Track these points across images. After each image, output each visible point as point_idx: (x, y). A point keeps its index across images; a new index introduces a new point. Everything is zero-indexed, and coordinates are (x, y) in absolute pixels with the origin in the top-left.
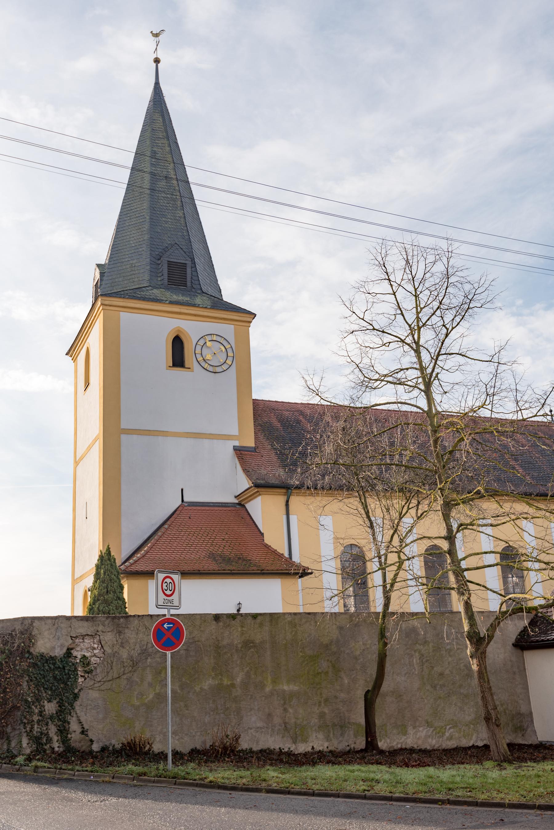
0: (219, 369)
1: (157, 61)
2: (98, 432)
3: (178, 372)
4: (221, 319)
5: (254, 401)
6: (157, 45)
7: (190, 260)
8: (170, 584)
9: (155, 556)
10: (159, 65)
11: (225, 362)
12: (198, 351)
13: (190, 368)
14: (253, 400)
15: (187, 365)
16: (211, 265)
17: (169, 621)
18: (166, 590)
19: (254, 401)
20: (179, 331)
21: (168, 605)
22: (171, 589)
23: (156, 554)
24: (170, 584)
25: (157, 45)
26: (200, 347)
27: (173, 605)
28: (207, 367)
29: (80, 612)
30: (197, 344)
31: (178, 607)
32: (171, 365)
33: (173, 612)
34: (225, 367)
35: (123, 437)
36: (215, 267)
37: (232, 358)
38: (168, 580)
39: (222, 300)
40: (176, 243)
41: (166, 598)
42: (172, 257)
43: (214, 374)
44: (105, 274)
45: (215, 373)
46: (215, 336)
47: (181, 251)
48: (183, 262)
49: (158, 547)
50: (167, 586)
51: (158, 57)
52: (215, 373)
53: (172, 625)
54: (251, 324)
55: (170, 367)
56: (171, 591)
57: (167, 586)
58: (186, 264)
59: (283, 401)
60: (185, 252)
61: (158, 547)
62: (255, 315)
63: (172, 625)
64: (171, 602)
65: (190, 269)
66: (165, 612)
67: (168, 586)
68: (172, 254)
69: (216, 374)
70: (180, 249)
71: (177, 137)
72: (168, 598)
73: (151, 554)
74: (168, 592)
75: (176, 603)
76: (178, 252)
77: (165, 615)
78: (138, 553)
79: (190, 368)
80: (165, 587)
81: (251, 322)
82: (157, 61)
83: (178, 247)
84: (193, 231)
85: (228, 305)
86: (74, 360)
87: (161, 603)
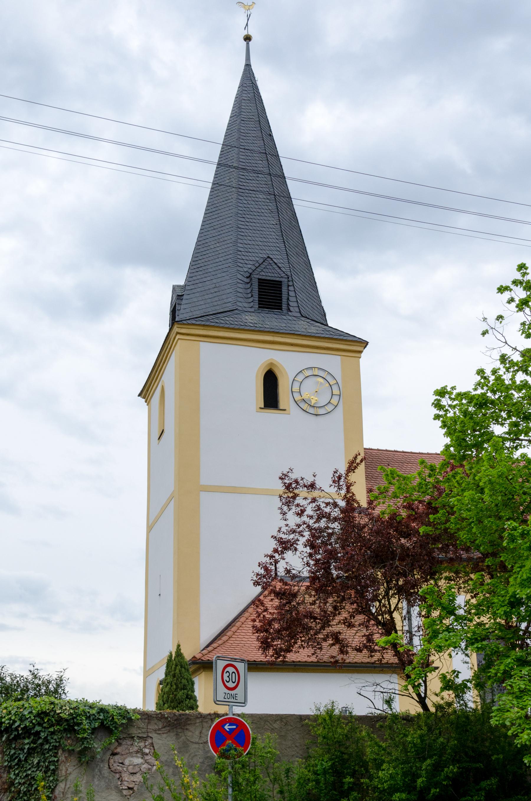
0: (321, 411)
1: (248, 38)
2: (172, 489)
3: (271, 414)
4: (292, 345)
5: (367, 451)
6: (248, 20)
7: (286, 277)
8: (234, 674)
9: (239, 642)
10: (250, 43)
11: (329, 402)
12: (296, 388)
13: (285, 410)
14: (365, 449)
15: (282, 405)
16: (313, 282)
17: (231, 721)
18: (228, 682)
19: (367, 451)
20: (272, 364)
21: (230, 700)
22: (234, 681)
23: (247, 640)
24: (234, 674)
25: (248, 20)
26: (298, 384)
27: (236, 701)
28: (307, 408)
29: (152, 707)
30: (294, 379)
31: (244, 703)
32: (263, 406)
33: (238, 710)
34: (329, 408)
35: (203, 495)
36: (318, 284)
37: (338, 397)
38: (231, 669)
39: (327, 325)
40: (268, 257)
41: (227, 691)
42: (263, 273)
43: (314, 417)
44: (184, 297)
45: (317, 415)
46: (316, 369)
47: (275, 266)
48: (278, 279)
49: (243, 631)
50: (228, 677)
51: (249, 33)
52: (317, 415)
53: (235, 727)
54: (362, 355)
55: (261, 408)
56: (234, 683)
57: (228, 677)
58: (281, 282)
59: (421, 452)
60: (280, 268)
61: (243, 631)
62: (367, 343)
63: (235, 727)
64: (234, 697)
65: (287, 288)
66: (222, 710)
67: (230, 677)
68: (264, 270)
69: (318, 417)
70: (274, 264)
71: (272, 128)
72: (230, 692)
73: (234, 639)
74: (231, 685)
75: (241, 699)
76: (271, 267)
77: (227, 714)
78: (220, 639)
79: (285, 410)
80: (226, 678)
81: (361, 352)
82: (248, 38)
83: (271, 262)
84: (291, 242)
85: (334, 331)
86: (148, 402)
87: (220, 697)
